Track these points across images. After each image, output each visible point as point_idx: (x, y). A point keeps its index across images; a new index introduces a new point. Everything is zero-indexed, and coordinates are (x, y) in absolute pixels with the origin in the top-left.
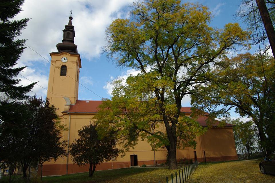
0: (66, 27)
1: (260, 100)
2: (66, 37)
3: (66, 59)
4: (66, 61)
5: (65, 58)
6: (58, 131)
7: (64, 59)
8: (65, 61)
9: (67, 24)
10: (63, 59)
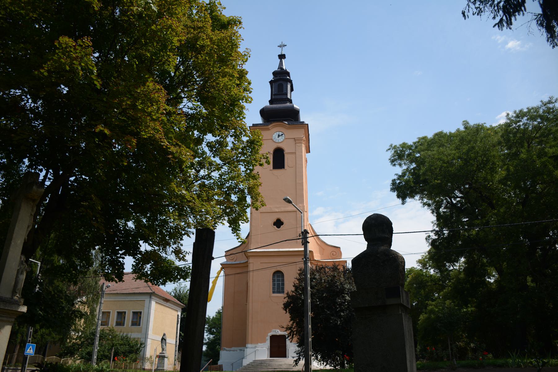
0: (274, 73)
1: (527, 154)
2: (275, 95)
3: (282, 135)
4: (282, 140)
5: (280, 133)
6: (75, 354)
7: (277, 136)
8: (281, 139)
9: (276, 68)
10: (275, 136)
